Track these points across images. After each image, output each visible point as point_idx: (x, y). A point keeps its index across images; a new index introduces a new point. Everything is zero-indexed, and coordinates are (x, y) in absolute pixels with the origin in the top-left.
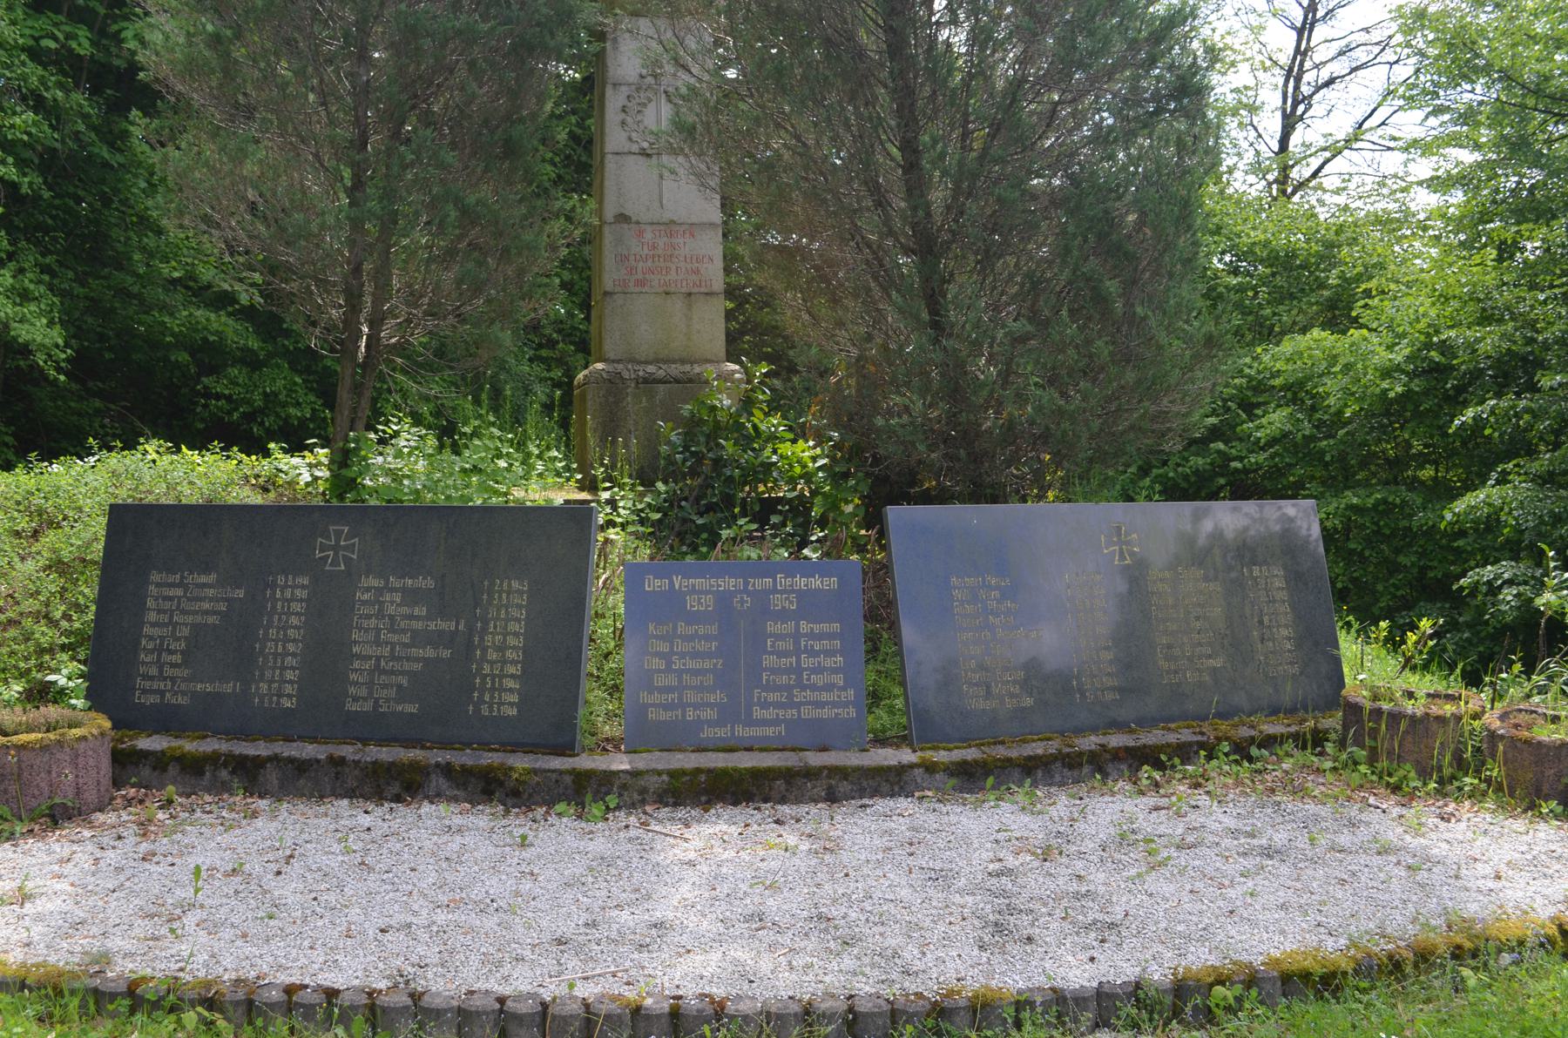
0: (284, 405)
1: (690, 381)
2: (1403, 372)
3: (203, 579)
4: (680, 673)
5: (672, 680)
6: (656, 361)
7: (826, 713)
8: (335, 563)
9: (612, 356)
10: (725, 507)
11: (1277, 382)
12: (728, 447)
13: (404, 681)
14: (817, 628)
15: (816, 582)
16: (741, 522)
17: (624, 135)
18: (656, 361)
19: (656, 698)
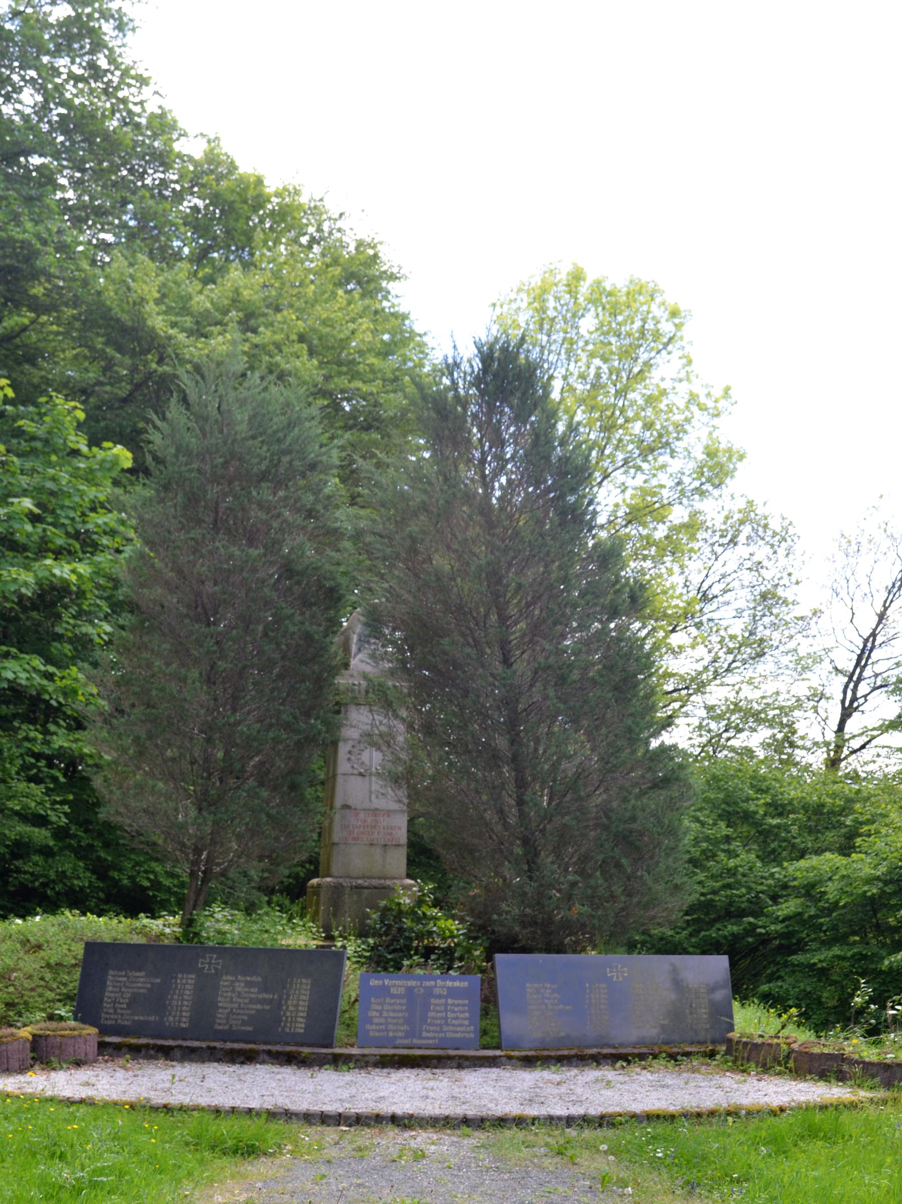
0: (70, 878)
1: (384, 888)
2: (881, 880)
3: (138, 974)
4: (386, 1018)
5: (383, 1021)
6: (363, 877)
7: (459, 1035)
8: (209, 969)
9: (336, 874)
10: (406, 951)
11: (795, 883)
12: (407, 923)
13: (246, 1018)
14: (456, 1002)
15: (457, 984)
16: (415, 958)
17: (348, 766)
18: (363, 877)
19: (374, 1027)
